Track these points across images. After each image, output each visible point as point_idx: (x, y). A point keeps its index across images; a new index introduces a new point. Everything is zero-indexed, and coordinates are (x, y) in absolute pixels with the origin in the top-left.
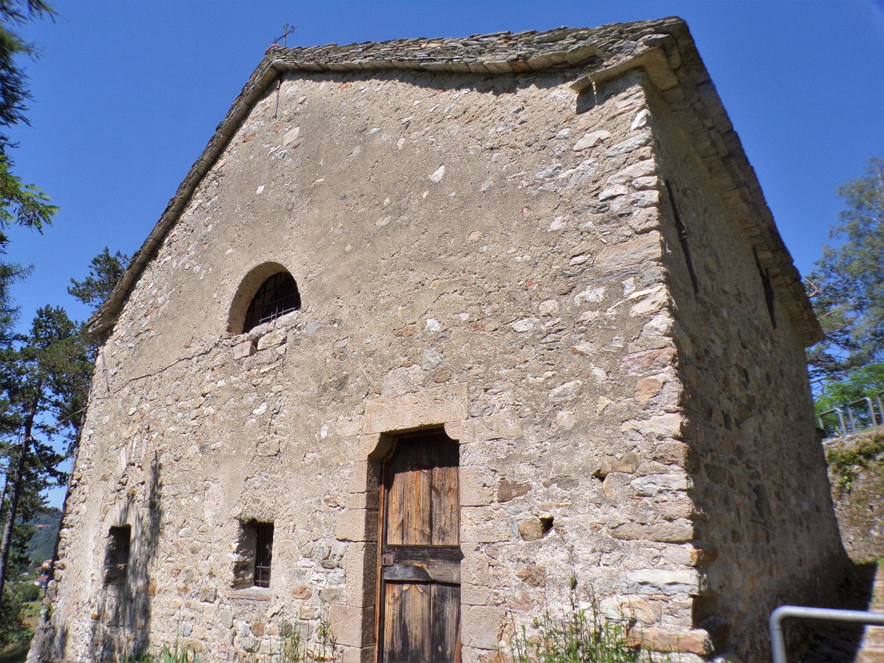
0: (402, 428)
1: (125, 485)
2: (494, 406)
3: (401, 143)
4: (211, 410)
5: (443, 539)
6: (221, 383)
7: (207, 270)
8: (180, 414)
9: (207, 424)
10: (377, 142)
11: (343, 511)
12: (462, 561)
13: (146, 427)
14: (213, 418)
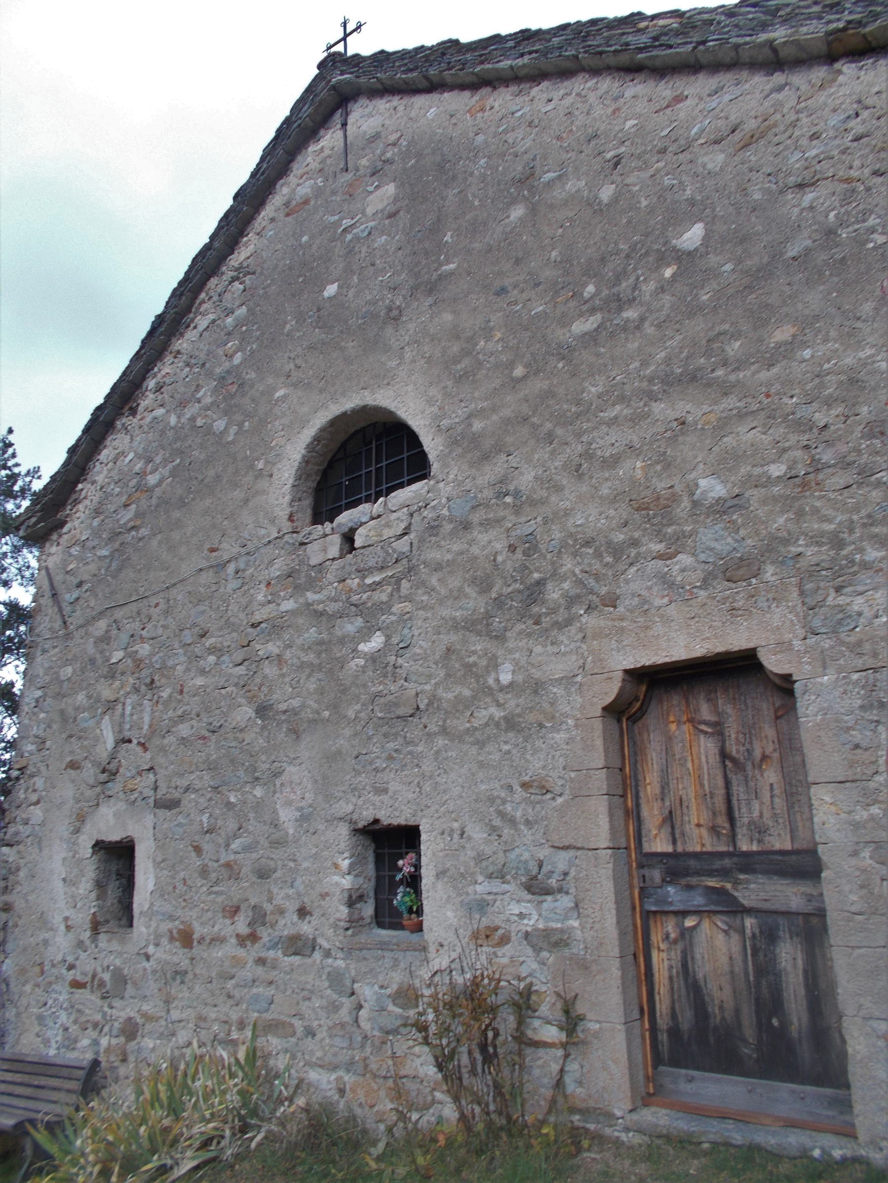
0: (667, 660)
1: (115, 774)
2: (860, 614)
3: (606, 193)
4: (273, 648)
5: (760, 841)
6: (288, 605)
7: (240, 425)
8: (212, 659)
9: (267, 671)
10: (558, 194)
11: (560, 800)
12: (823, 875)
13: (148, 680)
14: (280, 659)
